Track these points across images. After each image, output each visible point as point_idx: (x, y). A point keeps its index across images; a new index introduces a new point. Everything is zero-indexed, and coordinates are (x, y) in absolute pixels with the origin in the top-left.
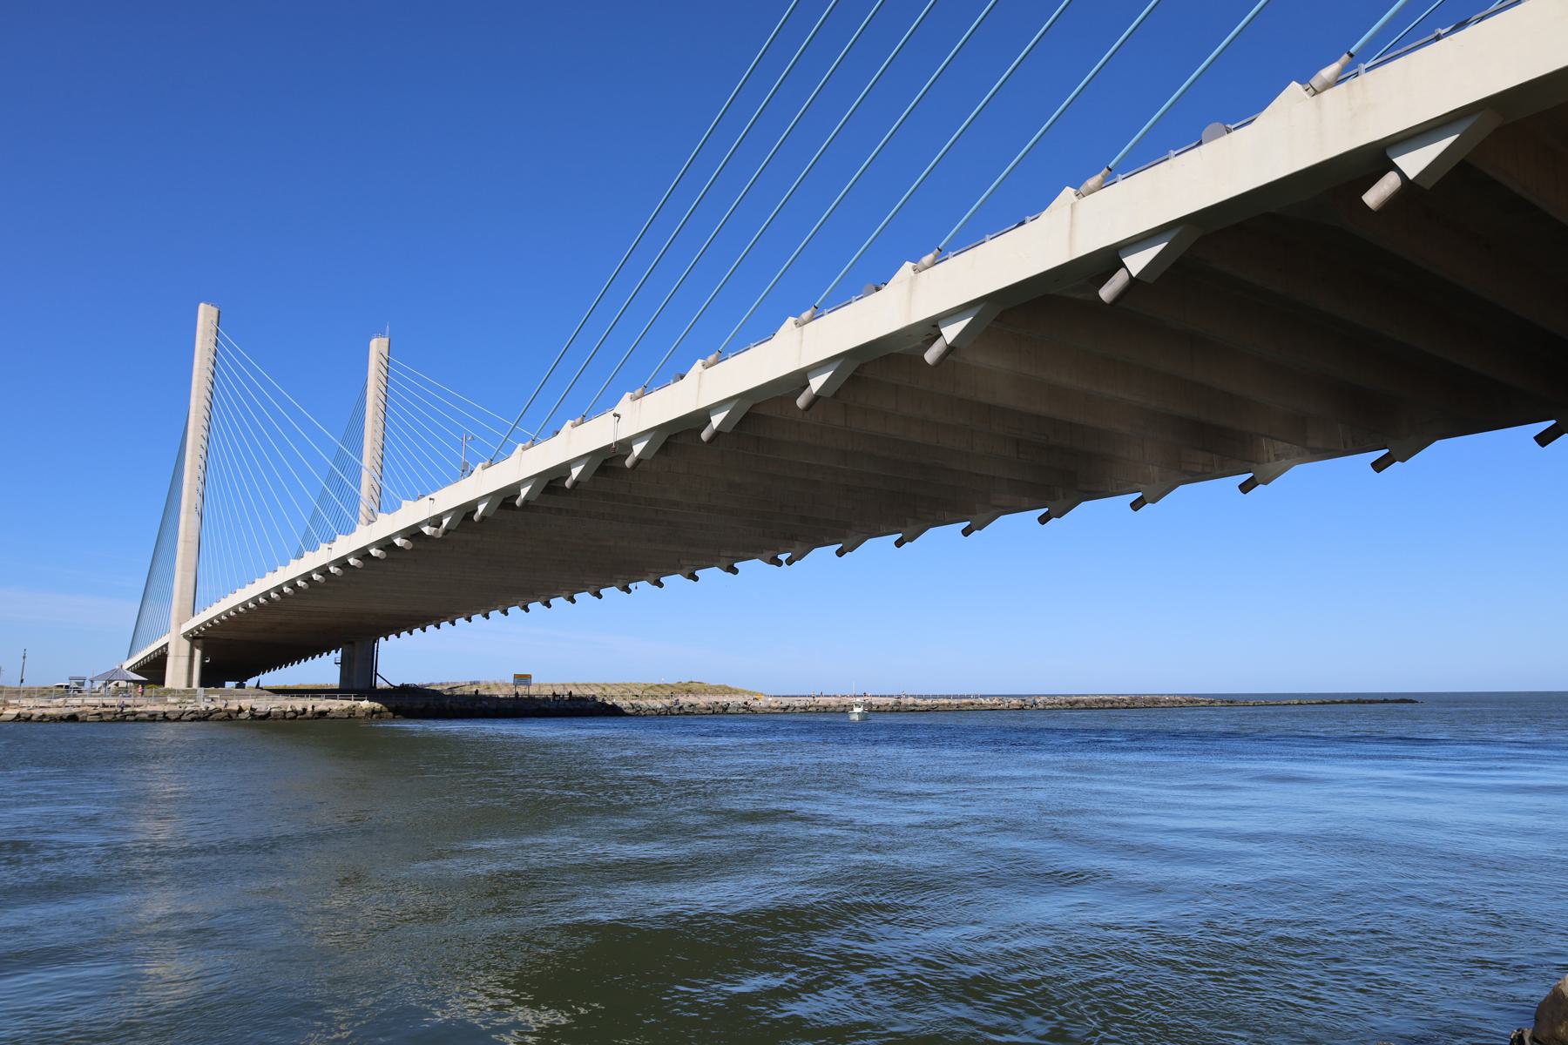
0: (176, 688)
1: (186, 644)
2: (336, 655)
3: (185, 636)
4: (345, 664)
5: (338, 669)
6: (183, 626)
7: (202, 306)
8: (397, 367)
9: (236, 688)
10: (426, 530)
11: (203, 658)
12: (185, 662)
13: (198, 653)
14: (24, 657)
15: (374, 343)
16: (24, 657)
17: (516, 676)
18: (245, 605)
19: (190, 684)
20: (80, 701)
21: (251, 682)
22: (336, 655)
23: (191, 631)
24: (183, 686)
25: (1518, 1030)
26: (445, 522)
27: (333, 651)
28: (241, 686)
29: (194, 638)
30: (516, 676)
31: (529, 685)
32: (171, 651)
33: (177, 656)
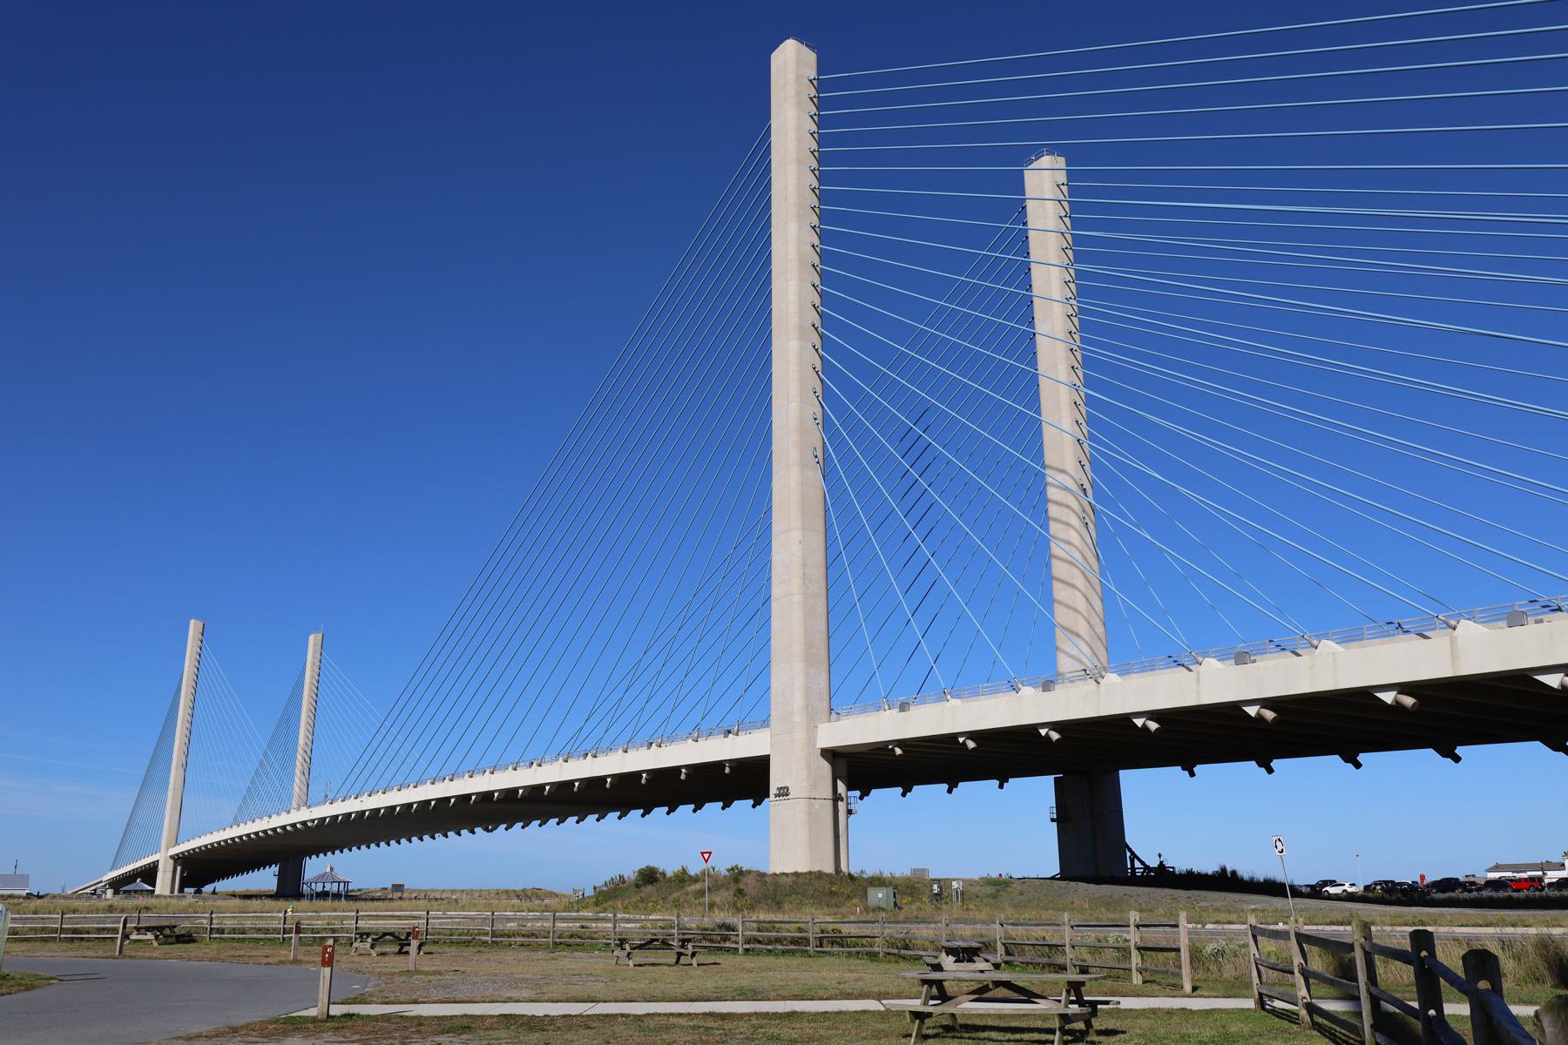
0: (164, 894)
1: (172, 861)
2: (275, 869)
3: (171, 857)
4: (281, 876)
5: (275, 880)
6: (170, 850)
7: (192, 622)
8: (327, 661)
9: (195, 893)
10: (309, 824)
11: (182, 872)
12: (169, 875)
13: (179, 868)
14: (16, 867)
15: (312, 638)
16: (16, 867)
17: (393, 885)
18: (219, 843)
19: (172, 892)
20: (809, 918)
21: (208, 889)
22: (275, 869)
23: (177, 855)
24: (167, 893)
25: (407, 953)
26: (316, 822)
27: (274, 866)
28: (199, 892)
29: (177, 859)
30: (393, 885)
31: (402, 891)
32: (161, 867)
33: (165, 872)
